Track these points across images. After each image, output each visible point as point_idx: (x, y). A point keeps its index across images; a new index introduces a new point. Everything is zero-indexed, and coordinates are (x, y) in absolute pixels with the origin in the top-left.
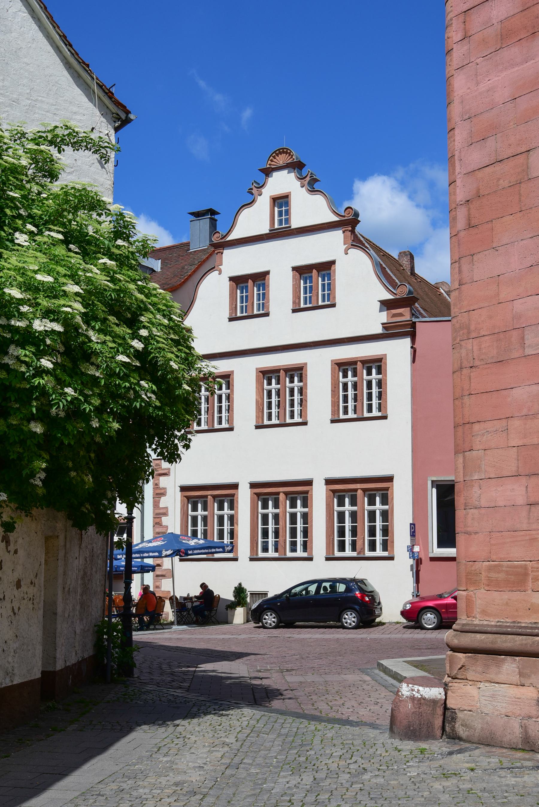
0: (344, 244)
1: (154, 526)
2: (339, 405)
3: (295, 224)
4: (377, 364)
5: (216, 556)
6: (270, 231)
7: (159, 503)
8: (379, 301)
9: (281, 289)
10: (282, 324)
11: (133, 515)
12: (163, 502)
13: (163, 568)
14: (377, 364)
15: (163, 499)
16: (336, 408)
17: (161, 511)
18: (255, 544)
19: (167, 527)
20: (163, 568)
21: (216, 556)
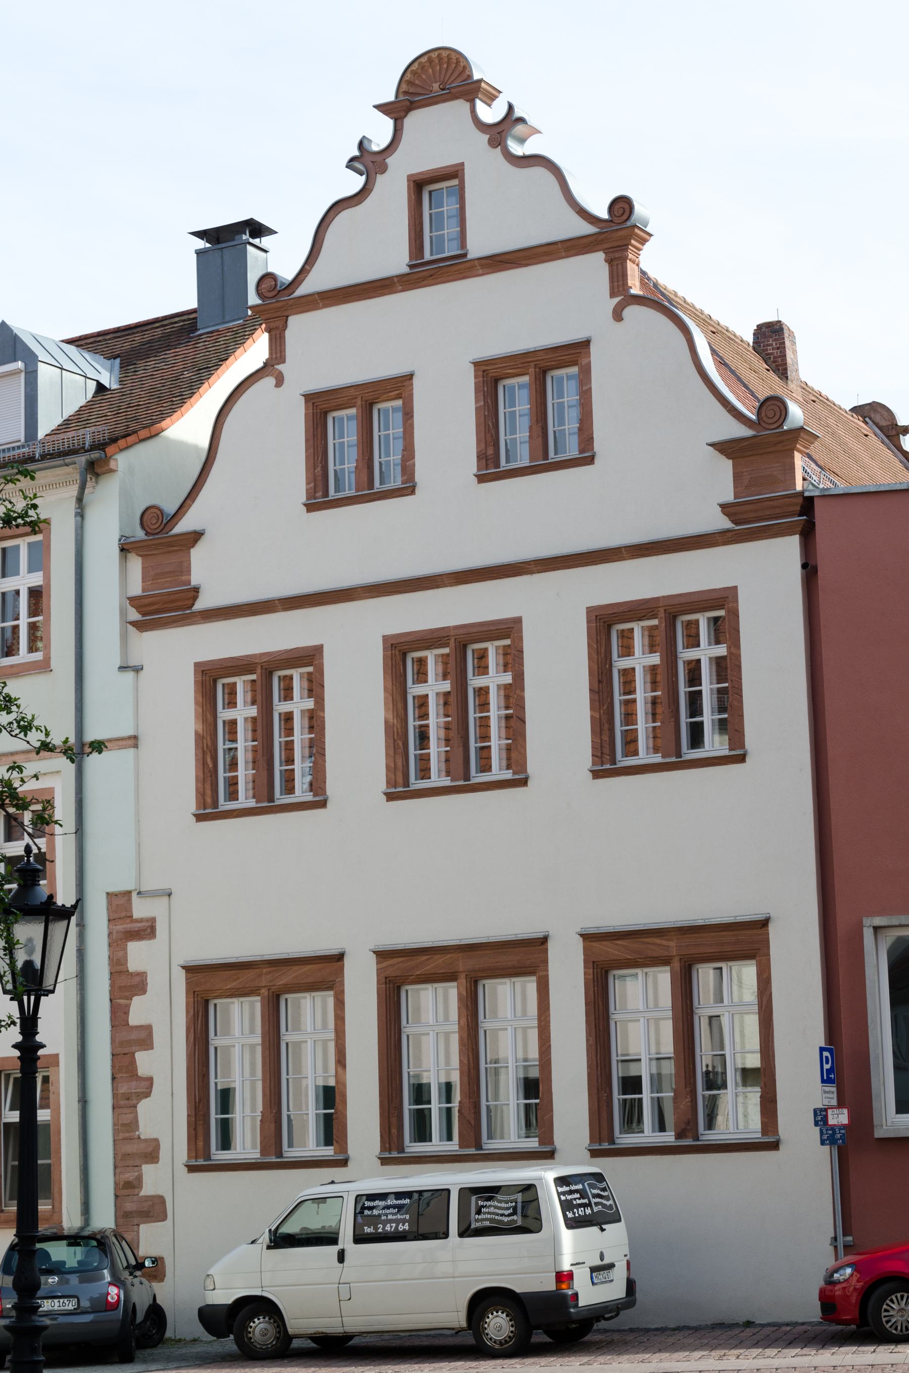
0: (613, 295)
1: (113, 1078)
2: (612, 730)
3: (477, 247)
4: (722, 608)
5: (408, 1334)
6: (411, 266)
7: (127, 1013)
8: (712, 445)
9: (445, 424)
10: (449, 513)
11: (38, 1038)
12: (140, 1011)
13: (142, 1193)
14: (722, 608)
15: (136, 1001)
16: (606, 738)
17: (134, 1036)
18: (394, 1120)
19: (150, 1080)
20: (142, 1193)
21: (768, 450)
